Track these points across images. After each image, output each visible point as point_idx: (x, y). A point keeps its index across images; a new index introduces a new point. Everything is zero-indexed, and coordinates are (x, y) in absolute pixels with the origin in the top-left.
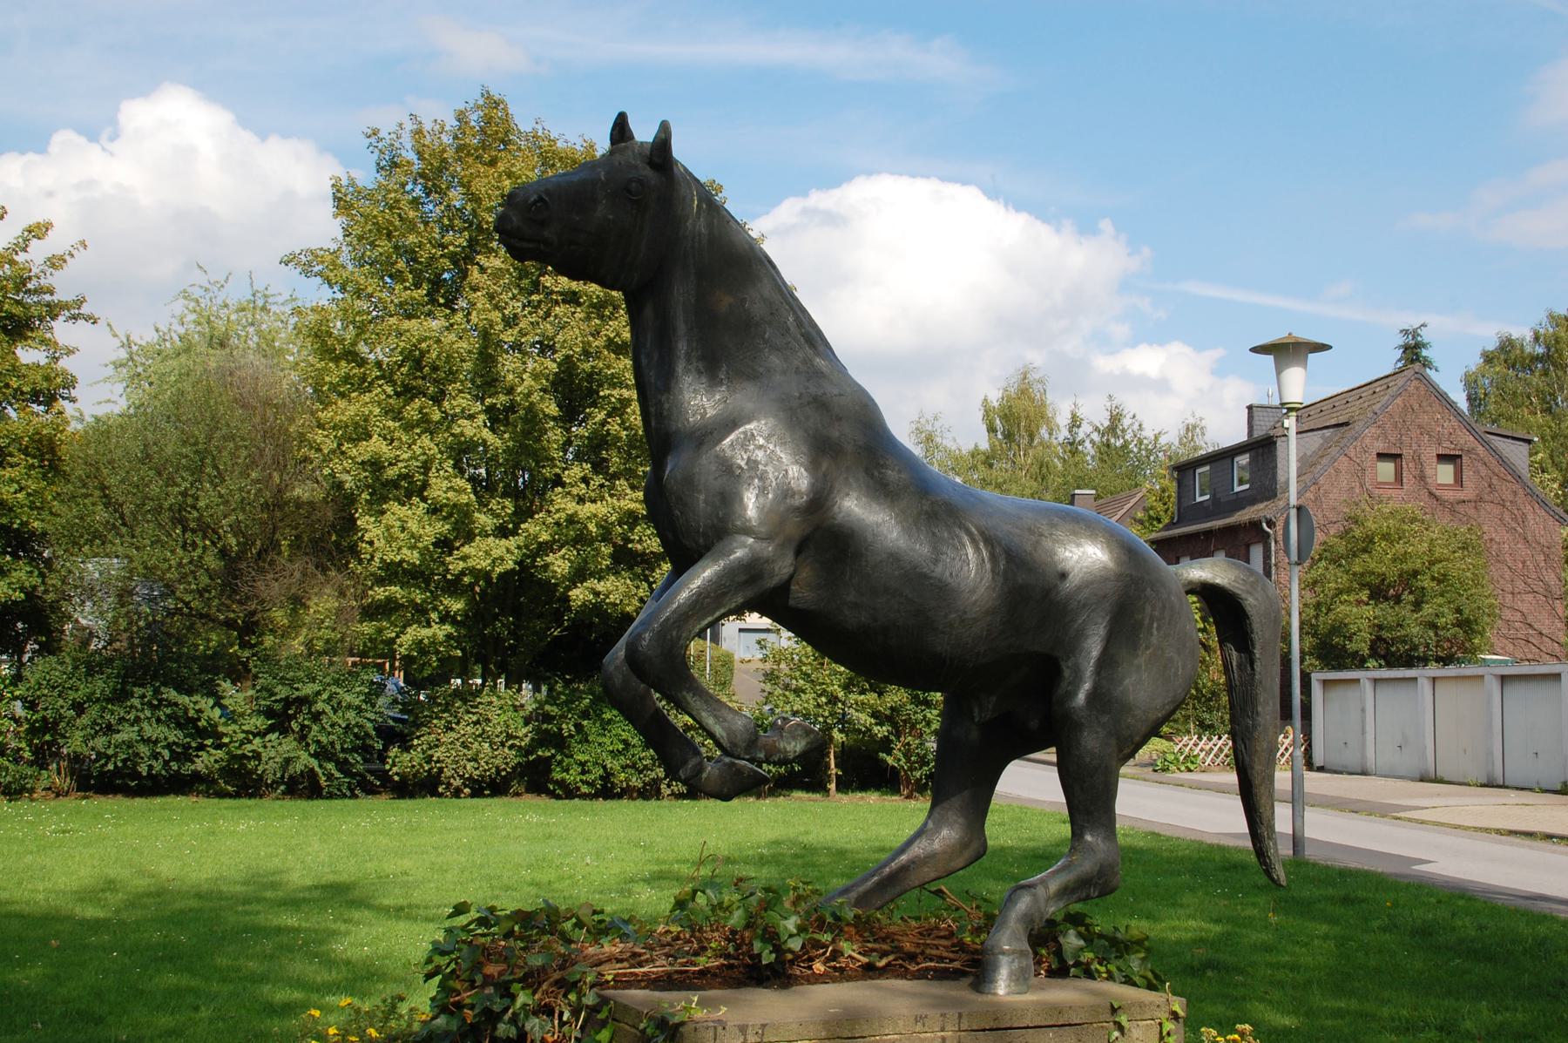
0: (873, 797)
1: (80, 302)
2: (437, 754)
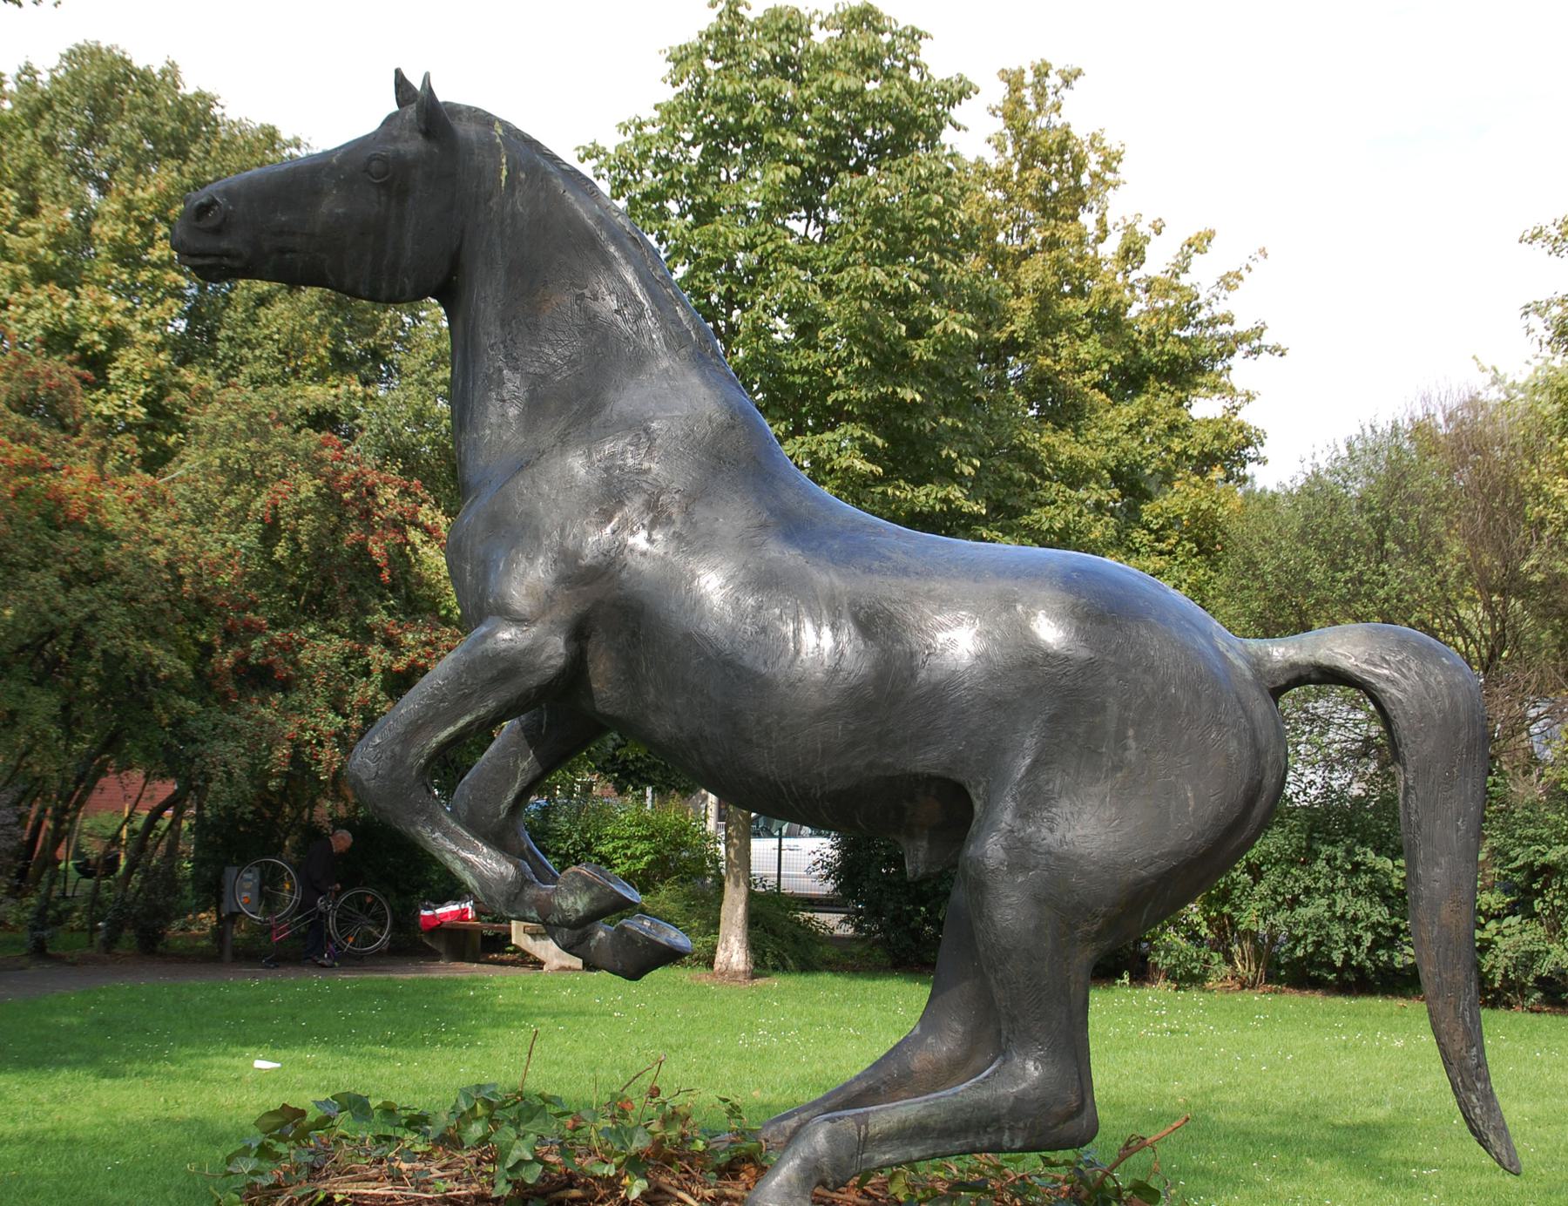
1: (1259, 332)
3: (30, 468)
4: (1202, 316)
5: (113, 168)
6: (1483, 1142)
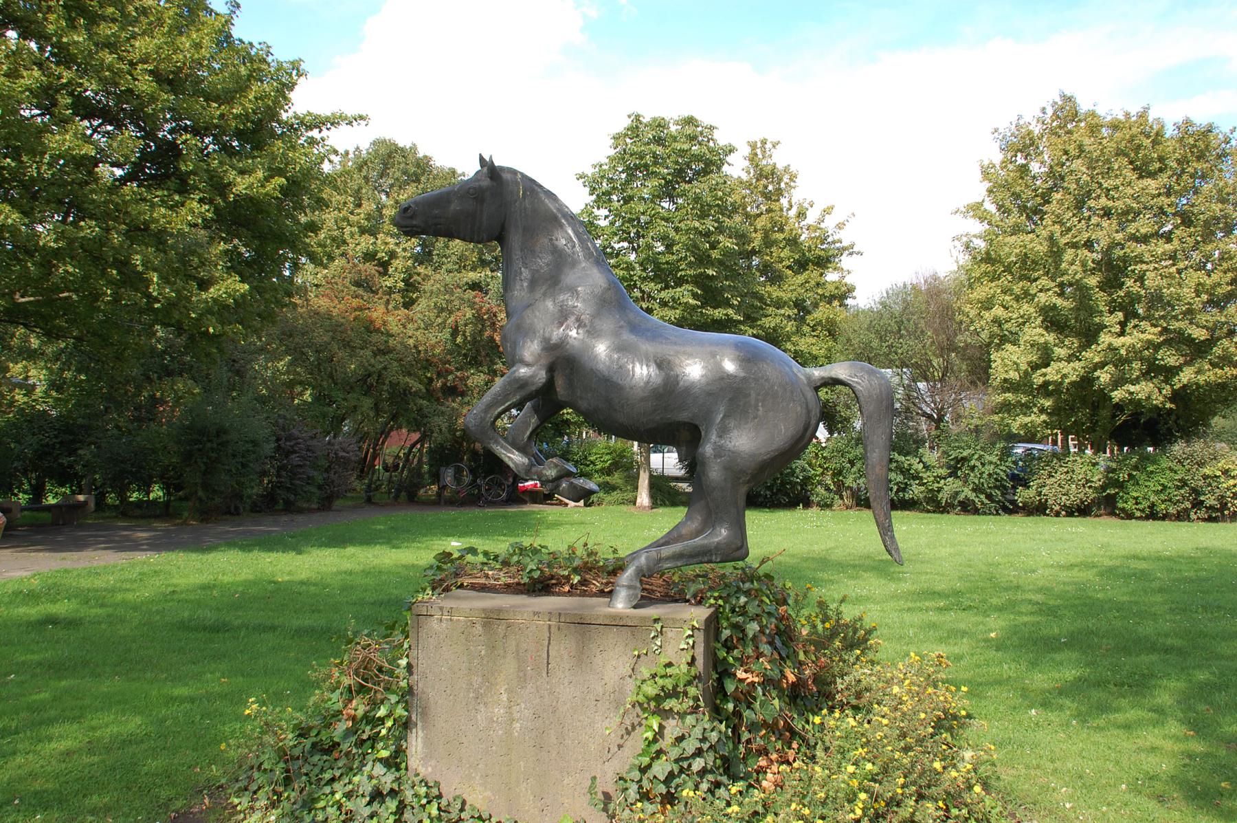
1: (852, 246)
2: (1044, 491)
3: (360, 309)
4: (830, 240)
5: (392, 186)
6: (890, 554)
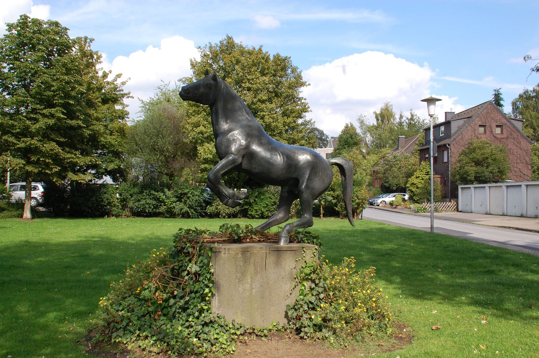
0: (332, 219)
1: (129, 94)
2: (219, 207)
